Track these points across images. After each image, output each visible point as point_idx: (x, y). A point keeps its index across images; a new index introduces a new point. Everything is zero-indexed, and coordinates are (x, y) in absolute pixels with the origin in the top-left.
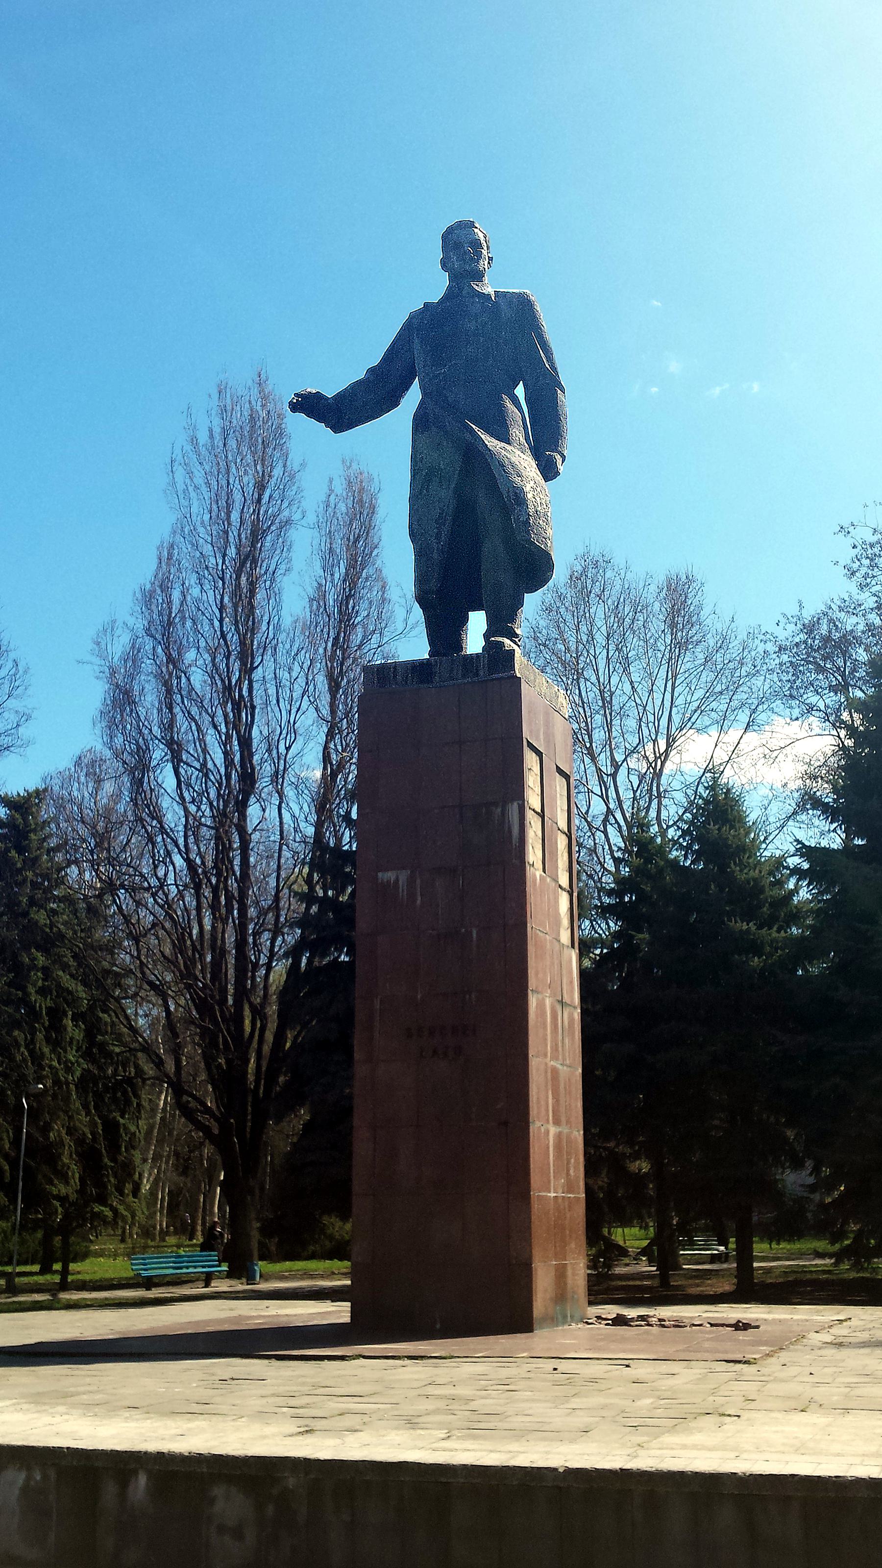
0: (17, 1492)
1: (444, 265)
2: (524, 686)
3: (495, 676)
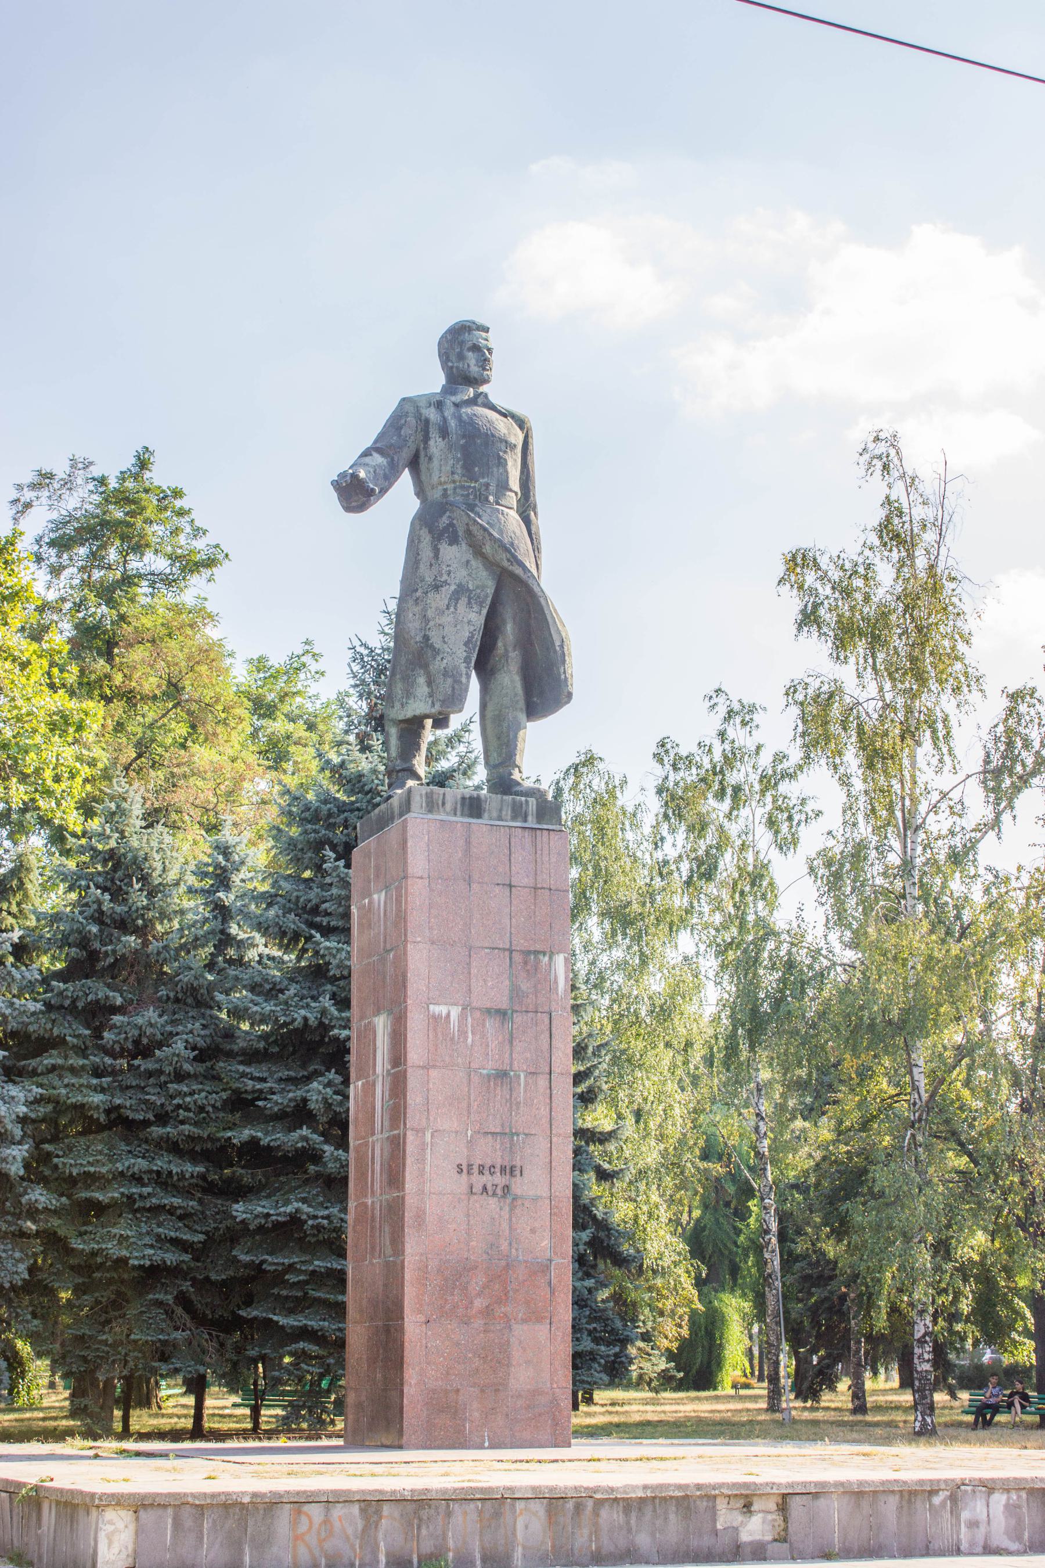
0: (1002, 1508)
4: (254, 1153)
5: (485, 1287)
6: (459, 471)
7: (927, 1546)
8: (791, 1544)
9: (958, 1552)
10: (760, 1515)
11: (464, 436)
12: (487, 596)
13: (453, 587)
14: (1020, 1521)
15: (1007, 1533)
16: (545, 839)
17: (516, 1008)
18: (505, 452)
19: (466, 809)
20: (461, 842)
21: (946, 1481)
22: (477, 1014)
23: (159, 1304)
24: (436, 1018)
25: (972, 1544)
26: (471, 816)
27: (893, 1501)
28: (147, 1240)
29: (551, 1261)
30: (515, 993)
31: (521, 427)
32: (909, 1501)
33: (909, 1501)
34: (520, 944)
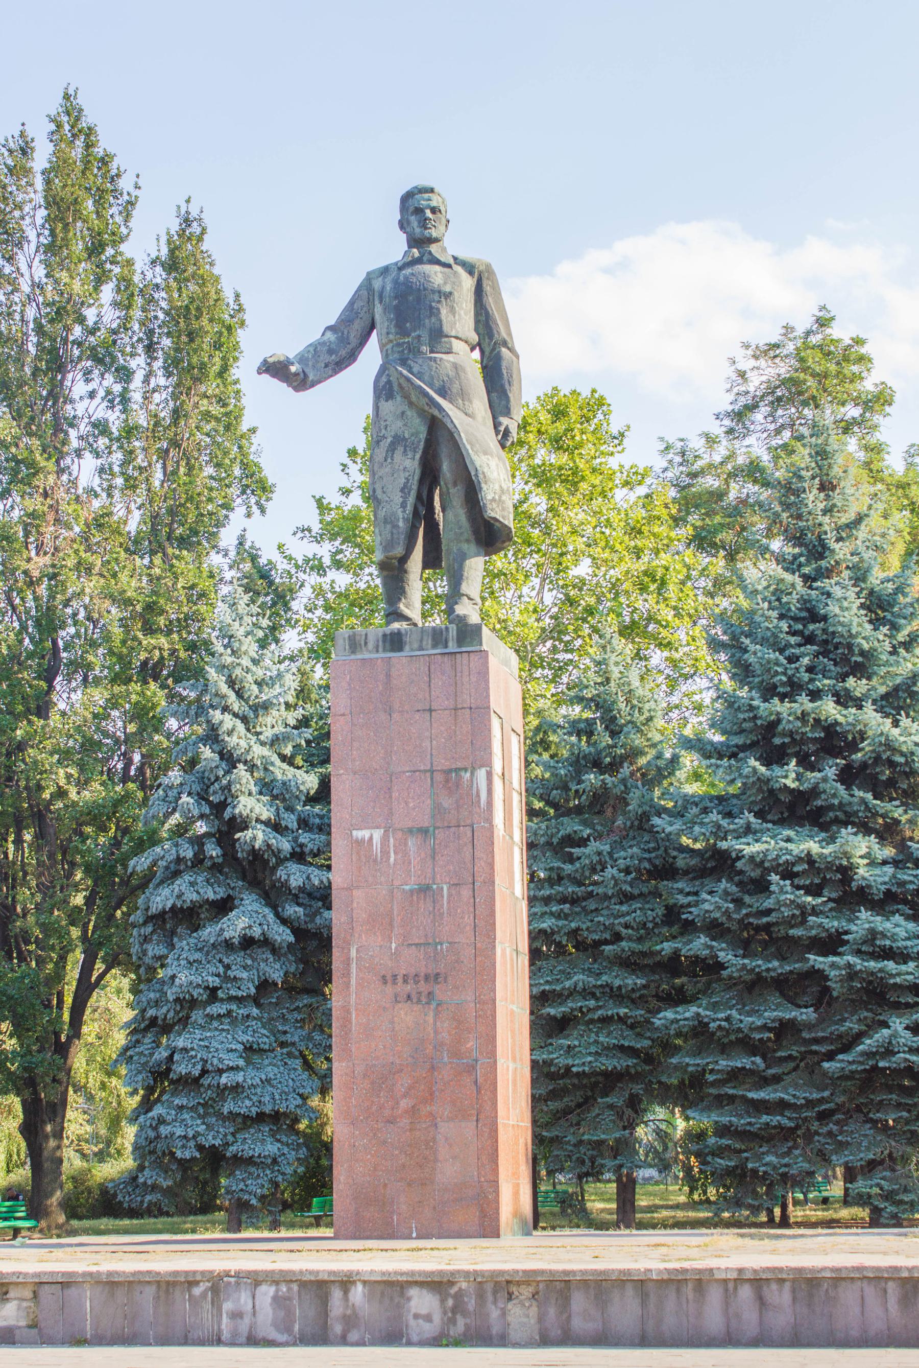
0: (269, 1300)
1: (402, 225)
2: (491, 657)
3: (464, 649)
4: (673, 965)
5: (411, 1088)
6: (393, 330)
7: (186, 1336)
8: (40, 1330)
9: (217, 1341)
10: (15, 1302)
11: (396, 297)
12: (419, 441)
13: (389, 440)
14: (289, 1313)
15: (275, 1325)
16: (465, 662)
17: (438, 824)
18: (439, 302)
19: (388, 645)
20: (382, 677)
21: (203, 1273)
22: (399, 835)
23: (611, 1107)
24: (359, 842)
25: (235, 1334)
26: (393, 650)
27: (150, 1291)
28: (593, 1049)
29: (477, 1061)
30: (438, 810)
31: (471, 273)
32: (167, 1291)
33: (167, 1291)
34: (442, 763)
